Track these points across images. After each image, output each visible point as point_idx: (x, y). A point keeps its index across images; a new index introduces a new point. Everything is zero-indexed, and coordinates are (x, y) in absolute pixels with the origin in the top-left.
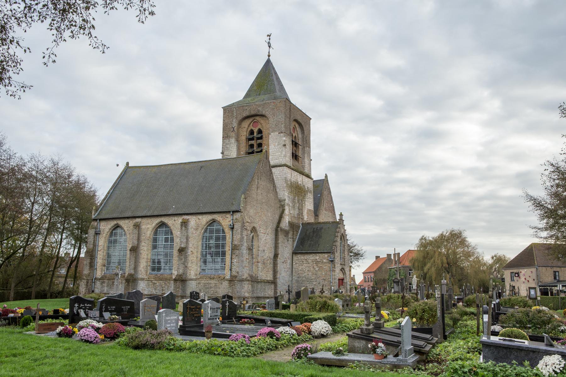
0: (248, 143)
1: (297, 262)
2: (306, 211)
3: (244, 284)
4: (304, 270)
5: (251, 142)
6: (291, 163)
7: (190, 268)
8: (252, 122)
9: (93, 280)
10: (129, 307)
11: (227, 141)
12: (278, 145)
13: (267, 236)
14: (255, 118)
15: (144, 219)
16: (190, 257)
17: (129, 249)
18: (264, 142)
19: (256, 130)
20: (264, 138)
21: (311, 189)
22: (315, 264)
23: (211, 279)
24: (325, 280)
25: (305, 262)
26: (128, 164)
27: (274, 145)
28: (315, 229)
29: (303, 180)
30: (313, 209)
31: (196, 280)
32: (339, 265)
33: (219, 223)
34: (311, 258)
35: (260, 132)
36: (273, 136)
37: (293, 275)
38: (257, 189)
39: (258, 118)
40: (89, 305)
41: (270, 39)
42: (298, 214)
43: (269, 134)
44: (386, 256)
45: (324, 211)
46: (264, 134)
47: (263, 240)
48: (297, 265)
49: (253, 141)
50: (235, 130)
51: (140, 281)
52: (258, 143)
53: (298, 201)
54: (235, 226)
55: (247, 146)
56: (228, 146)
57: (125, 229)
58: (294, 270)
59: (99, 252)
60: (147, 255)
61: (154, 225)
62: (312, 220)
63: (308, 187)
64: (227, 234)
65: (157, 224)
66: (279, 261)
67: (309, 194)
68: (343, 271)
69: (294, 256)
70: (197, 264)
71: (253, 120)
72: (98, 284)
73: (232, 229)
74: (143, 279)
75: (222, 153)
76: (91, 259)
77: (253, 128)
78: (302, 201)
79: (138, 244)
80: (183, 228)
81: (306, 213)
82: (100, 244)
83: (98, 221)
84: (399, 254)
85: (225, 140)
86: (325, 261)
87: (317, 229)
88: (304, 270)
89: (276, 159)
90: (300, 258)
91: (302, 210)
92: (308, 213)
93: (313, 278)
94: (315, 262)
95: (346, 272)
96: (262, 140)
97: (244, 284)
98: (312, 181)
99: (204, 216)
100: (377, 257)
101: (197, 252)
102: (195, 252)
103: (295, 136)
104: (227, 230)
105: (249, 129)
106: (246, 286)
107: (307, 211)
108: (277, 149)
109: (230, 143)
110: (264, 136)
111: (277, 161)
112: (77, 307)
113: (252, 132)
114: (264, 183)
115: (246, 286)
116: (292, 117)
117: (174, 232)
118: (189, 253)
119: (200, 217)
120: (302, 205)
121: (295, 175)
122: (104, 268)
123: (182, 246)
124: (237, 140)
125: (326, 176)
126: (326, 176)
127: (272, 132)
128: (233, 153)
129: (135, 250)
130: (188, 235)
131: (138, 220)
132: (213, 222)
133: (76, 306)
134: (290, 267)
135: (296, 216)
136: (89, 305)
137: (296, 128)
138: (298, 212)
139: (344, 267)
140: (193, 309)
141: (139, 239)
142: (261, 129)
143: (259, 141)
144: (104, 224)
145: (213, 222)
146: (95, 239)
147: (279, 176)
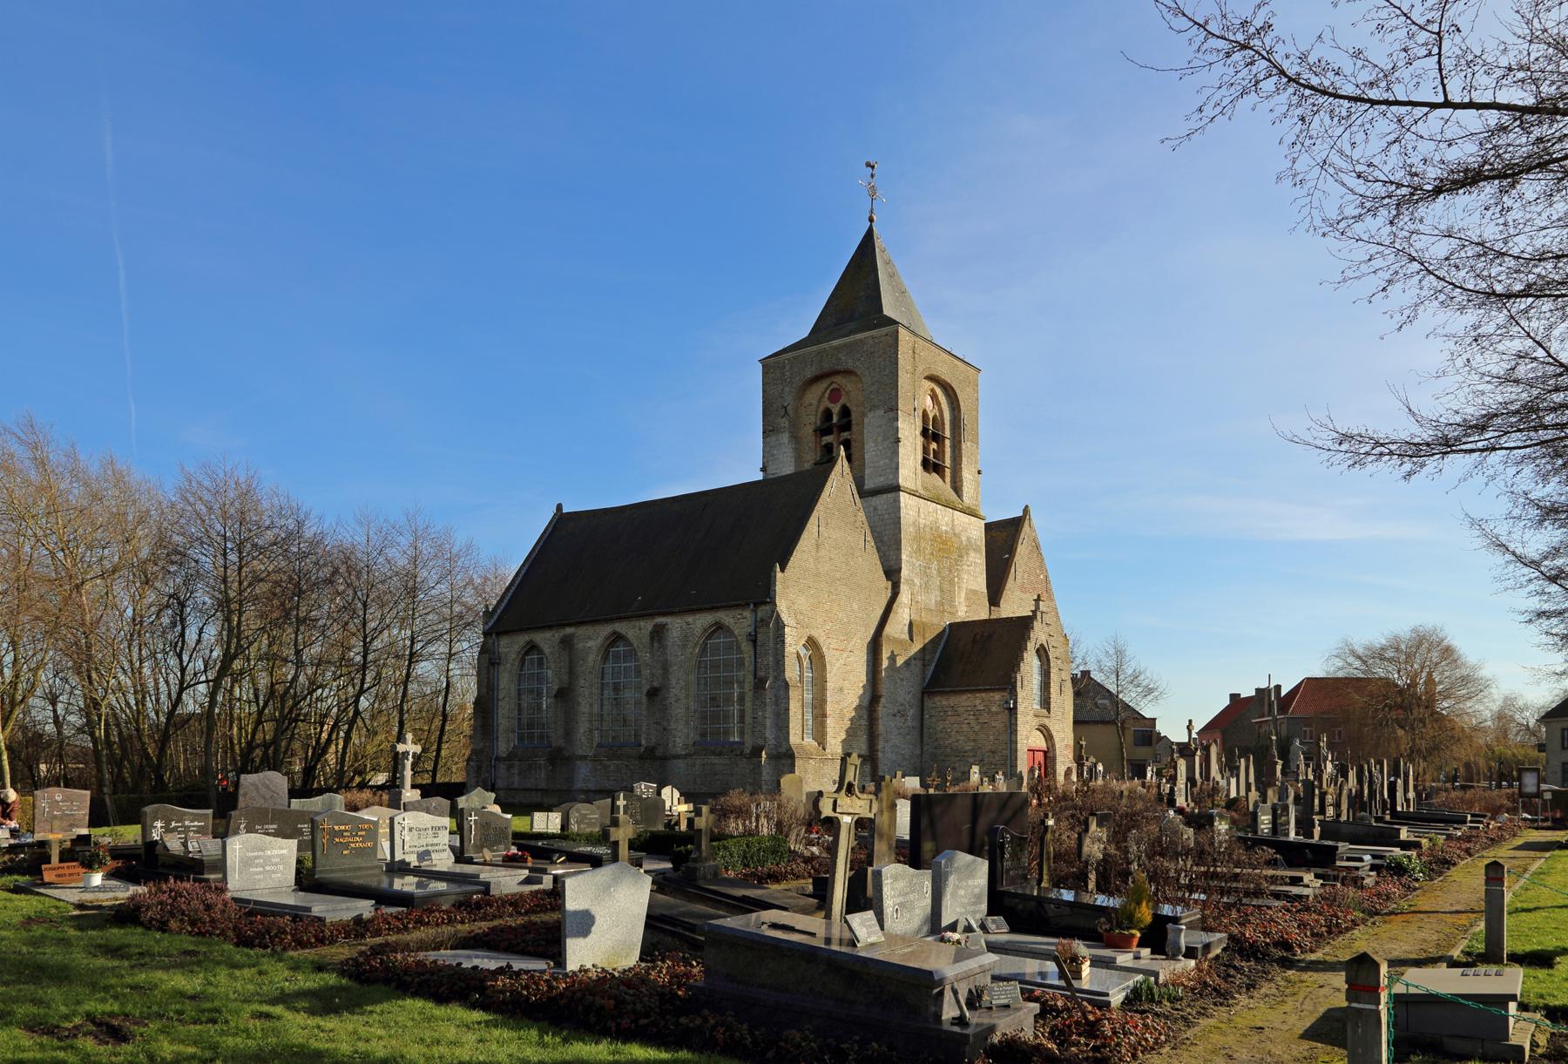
0: (821, 441)
1: (933, 712)
2: (963, 595)
5: (828, 439)
6: (919, 483)
7: (673, 732)
8: (827, 389)
10: (275, 826)
12: (884, 440)
14: (832, 379)
15: (698, 616)
19: (836, 409)
20: (854, 428)
21: (979, 543)
24: (993, 752)
25: (949, 713)
26: (559, 507)
28: (978, 637)
29: (953, 521)
31: (685, 757)
32: (1030, 718)
33: (728, 631)
34: (963, 704)
35: (845, 412)
37: (925, 742)
38: (818, 548)
39: (839, 380)
40: (196, 823)
41: (872, 176)
43: (864, 415)
44: (1253, 694)
45: (1018, 593)
47: (838, 665)
48: (934, 720)
52: (823, 443)
53: (939, 572)
55: (819, 449)
56: (775, 452)
58: (925, 730)
59: (500, 703)
60: (591, 705)
61: (599, 641)
62: (982, 613)
63: (968, 539)
65: (607, 639)
66: (882, 710)
67: (972, 554)
69: (926, 698)
70: (687, 723)
71: (830, 385)
72: (502, 767)
73: (755, 641)
74: (584, 758)
75: (764, 469)
76: (484, 717)
77: (831, 406)
78: (950, 570)
79: (570, 684)
80: (656, 645)
81: (962, 600)
82: (501, 687)
83: (494, 636)
84: (1278, 688)
86: (994, 709)
87: (982, 636)
91: (951, 592)
92: (967, 599)
93: (967, 748)
98: (983, 522)
100: (1234, 697)
101: (687, 696)
103: (935, 418)
104: (746, 647)
105: (822, 408)
110: (853, 422)
111: (882, 479)
112: (162, 827)
113: (828, 414)
116: (920, 368)
118: (672, 700)
120: (952, 582)
121: (931, 510)
122: (511, 735)
123: (656, 684)
124: (795, 438)
125: (1026, 510)
126: (1026, 510)
129: (564, 695)
130: (667, 660)
132: (718, 628)
134: (917, 724)
135: (933, 608)
136: (196, 823)
138: (939, 599)
140: (347, 831)
141: (572, 672)
142: (848, 405)
143: (845, 435)
145: (718, 628)
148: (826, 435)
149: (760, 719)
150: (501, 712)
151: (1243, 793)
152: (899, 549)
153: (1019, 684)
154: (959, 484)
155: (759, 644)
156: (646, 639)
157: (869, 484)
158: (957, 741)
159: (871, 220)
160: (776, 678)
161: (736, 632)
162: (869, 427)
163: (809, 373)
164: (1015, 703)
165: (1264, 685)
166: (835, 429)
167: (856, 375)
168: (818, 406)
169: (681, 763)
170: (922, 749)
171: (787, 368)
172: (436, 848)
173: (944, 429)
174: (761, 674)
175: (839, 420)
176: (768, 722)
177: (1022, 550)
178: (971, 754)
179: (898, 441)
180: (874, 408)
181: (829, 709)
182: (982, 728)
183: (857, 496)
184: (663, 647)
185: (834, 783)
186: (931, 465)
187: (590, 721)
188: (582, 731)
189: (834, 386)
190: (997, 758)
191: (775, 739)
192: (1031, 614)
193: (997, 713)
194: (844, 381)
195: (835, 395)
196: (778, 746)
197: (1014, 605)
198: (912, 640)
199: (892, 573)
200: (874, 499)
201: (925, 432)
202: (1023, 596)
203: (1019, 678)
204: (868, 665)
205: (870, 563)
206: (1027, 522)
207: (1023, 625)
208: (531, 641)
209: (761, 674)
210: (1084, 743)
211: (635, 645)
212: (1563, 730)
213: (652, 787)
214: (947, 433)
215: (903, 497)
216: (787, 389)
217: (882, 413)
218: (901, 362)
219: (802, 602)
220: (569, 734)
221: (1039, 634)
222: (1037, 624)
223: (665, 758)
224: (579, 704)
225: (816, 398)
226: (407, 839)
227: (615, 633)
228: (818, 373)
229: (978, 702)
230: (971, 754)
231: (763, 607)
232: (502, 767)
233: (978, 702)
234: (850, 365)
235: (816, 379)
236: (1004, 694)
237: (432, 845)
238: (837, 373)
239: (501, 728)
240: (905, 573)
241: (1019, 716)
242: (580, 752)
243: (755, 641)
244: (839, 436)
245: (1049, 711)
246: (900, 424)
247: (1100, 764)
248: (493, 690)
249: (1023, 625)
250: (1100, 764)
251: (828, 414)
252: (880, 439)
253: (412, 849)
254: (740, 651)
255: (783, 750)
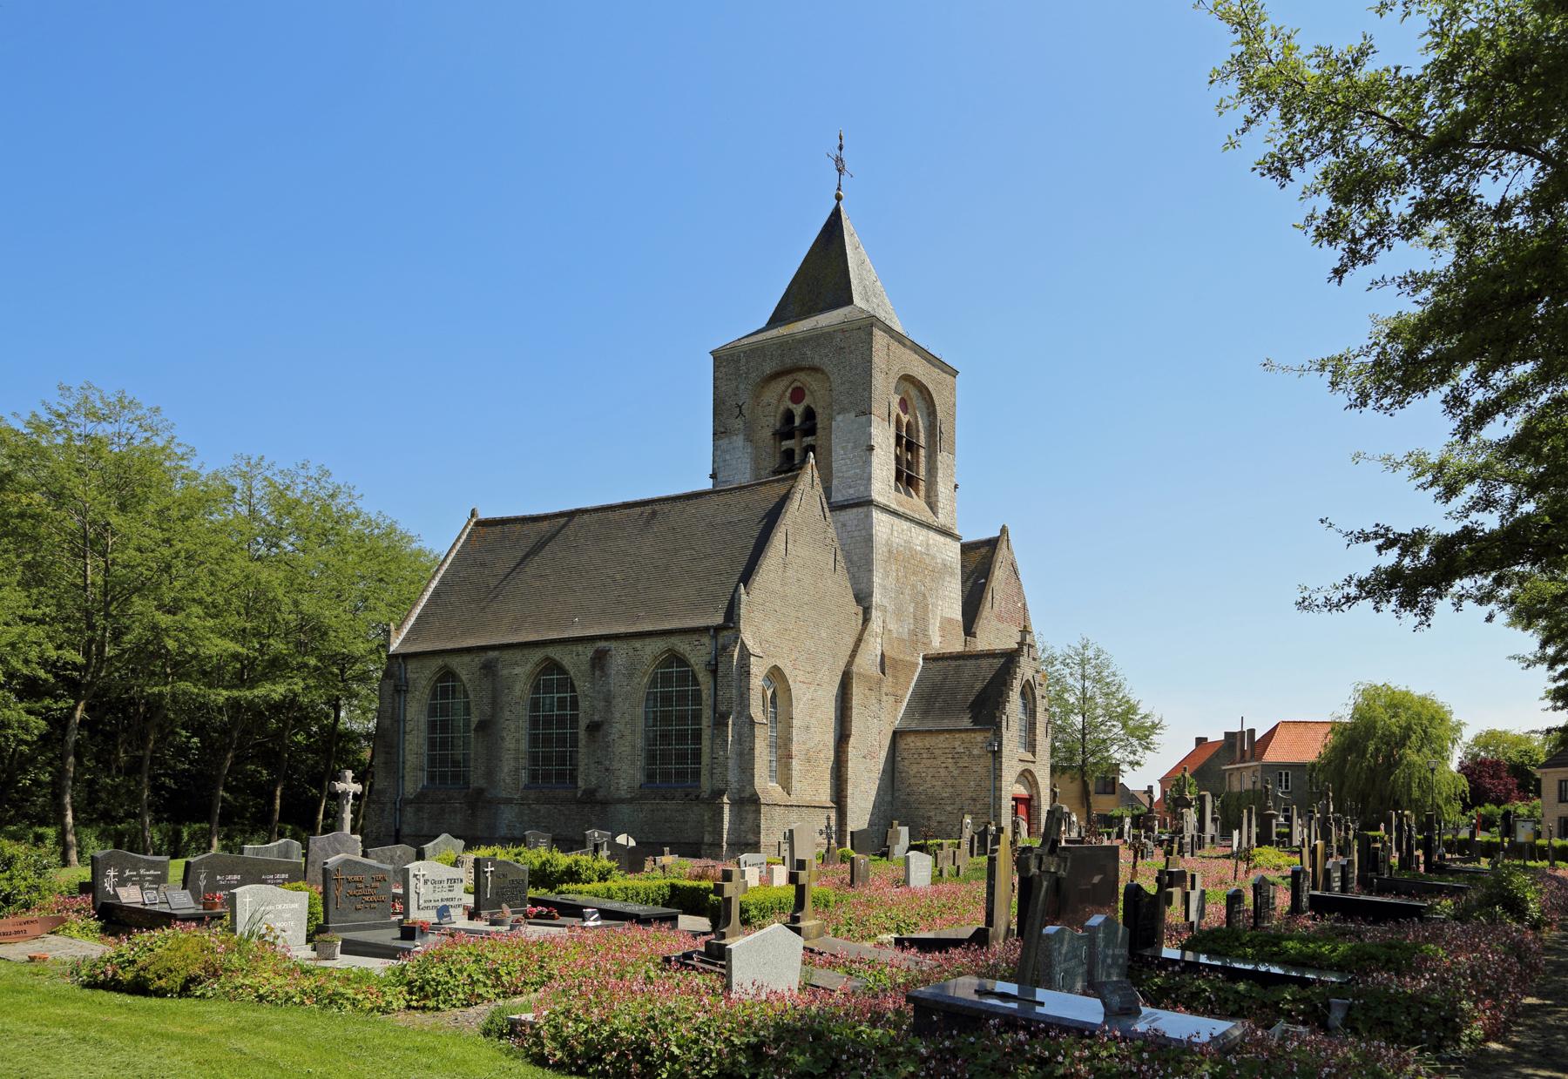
0: (781, 446)
3: (746, 811)
4: (924, 775)
5: (787, 444)
8: (787, 388)
9: (395, 803)
11: (724, 442)
12: (854, 448)
13: (815, 691)
14: (795, 376)
15: (505, 652)
16: (616, 745)
17: (473, 726)
18: (820, 442)
19: (798, 410)
20: (820, 432)
22: (950, 760)
23: (666, 799)
24: (974, 800)
25: (925, 756)
27: (843, 448)
30: (960, 618)
31: (631, 801)
32: (1015, 762)
34: (940, 746)
35: (810, 414)
36: (841, 424)
39: (803, 378)
40: (152, 872)
42: (914, 633)
45: (994, 623)
46: (820, 421)
49: (793, 441)
50: (743, 411)
51: (502, 806)
52: (804, 444)
54: (720, 665)
55: (778, 455)
56: (728, 457)
57: (464, 678)
58: (897, 775)
59: (407, 737)
60: (518, 741)
61: (529, 667)
62: (957, 646)
64: (703, 687)
68: (1030, 778)
70: (633, 763)
72: (409, 811)
73: (714, 672)
74: (509, 801)
75: (713, 476)
77: (792, 406)
80: (597, 673)
83: (400, 660)
84: (1252, 732)
85: (720, 442)
86: (975, 752)
88: (924, 775)
89: (850, 487)
90: (912, 744)
92: (942, 628)
93: (945, 795)
94: (950, 756)
95: (1039, 780)
96: (814, 437)
97: (746, 811)
99: (647, 641)
100: (1200, 741)
101: (633, 732)
102: (627, 732)
103: (908, 424)
104: (704, 679)
105: (782, 408)
106: (749, 816)
107: (941, 623)
108: (851, 460)
109: (734, 448)
110: (819, 426)
111: (851, 491)
113: (789, 416)
114: (807, 553)
115: (749, 816)
117: (576, 683)
119: (638, 644)
122: (420, 774)
123: (596, 718)
125: (1004, 530)
126: (1004, 530)
127: (839, 414)
128: (742, 473)
130: (609, 691)
131: (492, 654)
133: (112, 874)
136: (152, 872)
137: (911, 399)
138: (912, 627)
139: (1031, 766)
141: (495, 702)
143: (809, 440)
144: (414, 666)
146: (397, 705)
147: (856, 533)
148: (787, 439)
149: (721, 759)
150: (408, 747)
151: (1245, 845)
152: (871, 571)
153: (1004, 724)
154: (933, 499)
155: (720, 674)
156: (585, 667)
157: (837, 497)
158: (933, 787)
159: (839, 198)
160: (740, 714)
161: (692, 661)
162: (840, 426)
163: (769, 368)
164: (1000, 745)
165: (1237, 729)
166: (797, 433)
167: (823, 372)
168: (777, 407)
169: (625, 809)
170: (893, 795)
171: (743, 361)
172: (451, 903)
173: (918, 436)
174: (723, 708)
175: (802, 423)
176: (731, 763)
177: (999, 574)
178: (949, 802)
179: (871, 448)
180: (843, 410)
181: (795, 748)
182: (963, 773)
183: (827, 510)
184: (605, 674)
185: (821, 833)
186: (906, 478)
187: (517, 759)
188: (506, 770)
189: (797, 384)
190: (979, 807)
191: (738, 782)
192: (1016, 646)
193: (979, 757)
194: (809, 379)
195: (798, 395)
196: (741, 790)
197: (994, 636)
198: (883, 673)
199: (863, 599)
200: (843, 513)
201: (899, 438)
202: (1001, 626)
203: (1004, 717)
204: (836, 701)
205: (839, 587)
206: (1004, 546)
207: (1010, 659)
208: (446, 666)
209: (723, 708)
210: (1058, 790)
211: (572, 673)
212: (1561, 782)
213: (606, 836)
214: (922, 442)
215: (877, 515)
216: (742, 387)
217: (852, 415)
218: (875, 359)
219: (769, 628)
220: (490, 774)
221: (1025, 670)
222: (1023, 660)
223: (605, 803)
224: (503, 739)
225: (776, 398)
226: (422, 891)
227: (547, 658)
228: (779, 368)
229: (957, 744)
230: (949, 802)
231: (725, 633)
232: (409, 811)
233: (957, 744)
234: (817, 361)
235: (776, 375)
236: (987, 735)
237: (447, 899)
238: (801, 369)
239: (408, 764)
240: (877, 598)
241: (1004, 760)
242: (504, 794)
243: (714, 672)
244: (801, 442)
245: (1034, 754)
246: (874, 431)
247: (1074, 814)
248: (398, 721)
249: (1010, 659)
250: (1074, 814)
251: (789, 416)
252: (850, 445)
253: (426, 905)
254: (696, 682)
255: (747, 794)
